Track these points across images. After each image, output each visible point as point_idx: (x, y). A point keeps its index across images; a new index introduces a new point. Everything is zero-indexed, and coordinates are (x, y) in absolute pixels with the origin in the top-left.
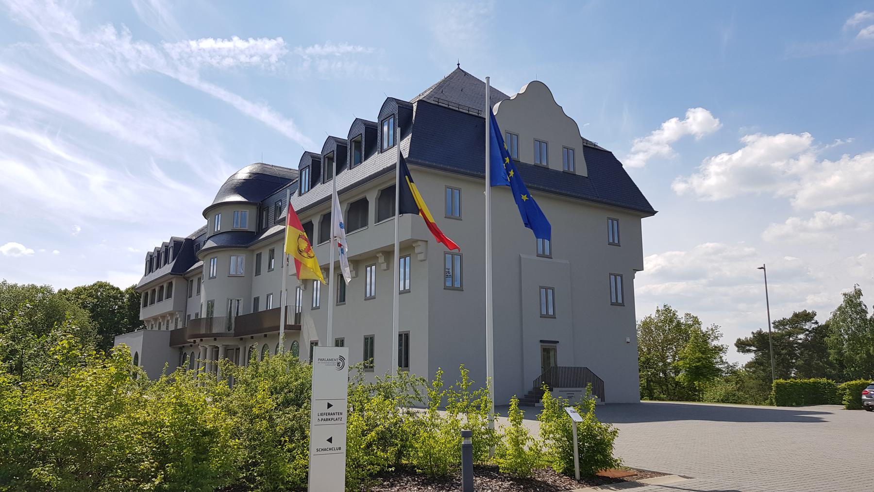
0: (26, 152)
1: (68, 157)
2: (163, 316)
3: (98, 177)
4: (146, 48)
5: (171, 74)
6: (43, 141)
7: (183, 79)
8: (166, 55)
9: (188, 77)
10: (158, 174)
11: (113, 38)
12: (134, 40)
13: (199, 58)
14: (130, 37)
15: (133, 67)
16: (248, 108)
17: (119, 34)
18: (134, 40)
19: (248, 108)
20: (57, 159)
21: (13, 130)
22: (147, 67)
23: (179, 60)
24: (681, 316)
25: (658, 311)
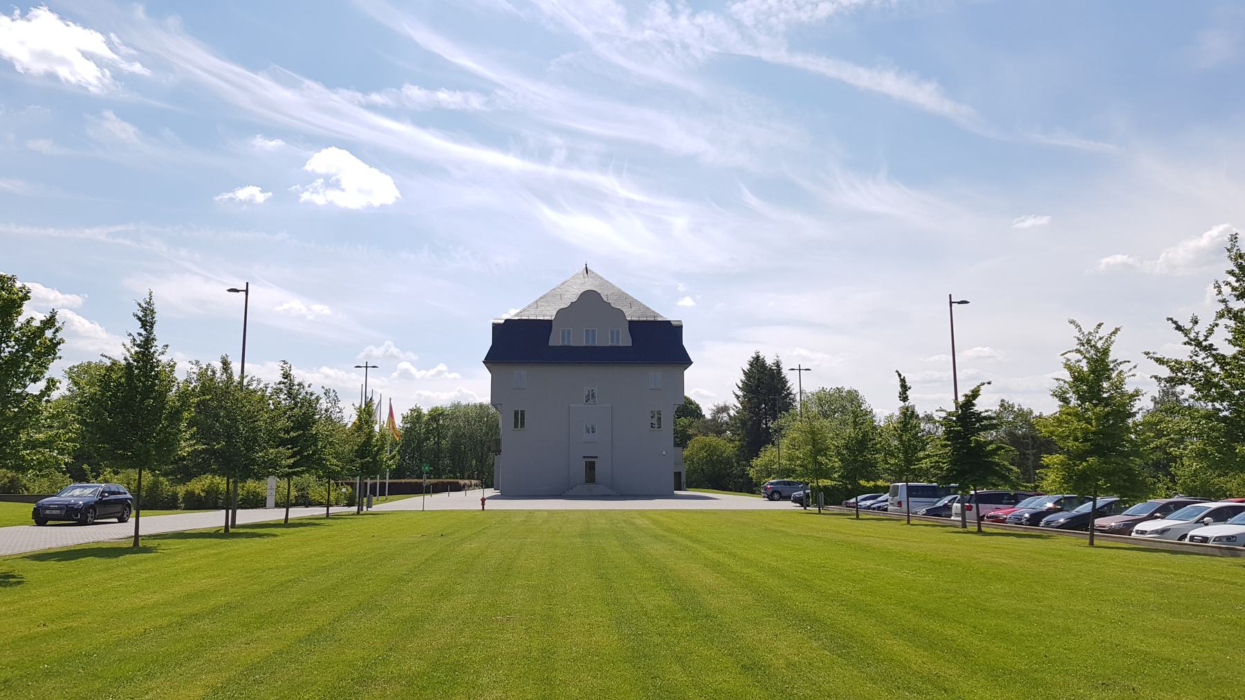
0: (593, 200)
1: (637, 197)
2: (337, 504)
3: (680, 220)
4: (707, 20)
5: (748, 51)
6: (607, 181)
7: (766, 55)
8: (739, 25)
9: (774, 53)
10: (752, 200)
11: (668, 19)
12: (693, 15)
13: (782, 16)
14: (688, 11)
15: (698, 54)
16: (863, 78)
17: (674, 13)
18: (693, 15)
19: (863, 78)
20: (630, 203)
21: (576, 174)
22: (716, 50)
23: (755, 26)
24: (769, 361)
25: (1230, 341)
